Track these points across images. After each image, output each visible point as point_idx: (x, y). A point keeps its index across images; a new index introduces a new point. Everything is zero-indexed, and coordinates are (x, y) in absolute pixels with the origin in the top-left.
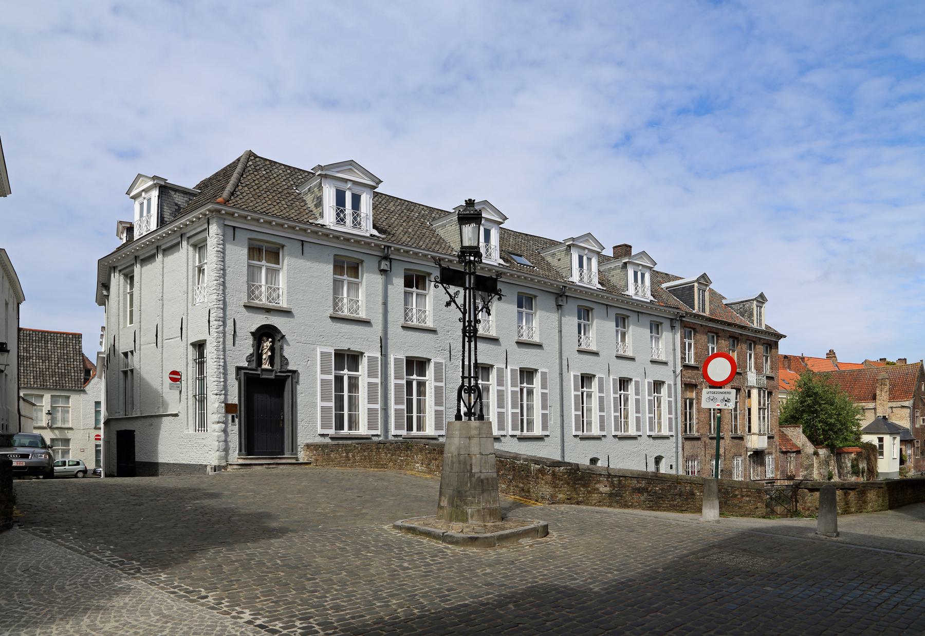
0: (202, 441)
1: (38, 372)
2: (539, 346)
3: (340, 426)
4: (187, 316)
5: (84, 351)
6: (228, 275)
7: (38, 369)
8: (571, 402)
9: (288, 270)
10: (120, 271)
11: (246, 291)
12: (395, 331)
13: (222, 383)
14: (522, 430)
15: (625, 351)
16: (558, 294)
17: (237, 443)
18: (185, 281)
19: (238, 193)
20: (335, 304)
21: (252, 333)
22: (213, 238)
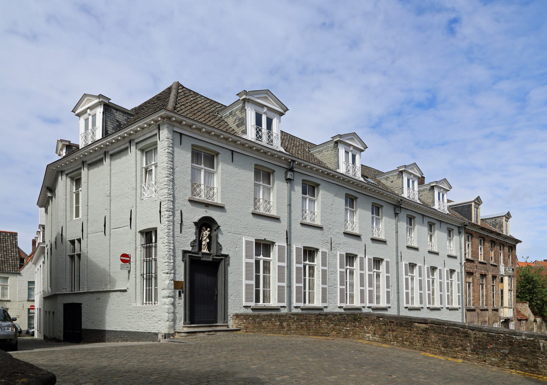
0: (152, 312)
3: (257, 300)
4: (136, 208)
5: (20, 245)
6: (176, 174)
8: (403, 283)
9: (222, 173)
10: (67, 175)
12: (296, 227)
13: (172, 264)
14: (305, 302)
16: (396, 205)
17: (183, 314)
18: (134, 179)
19: (179, 109)
21: (195, 223)
22: (164, 142)
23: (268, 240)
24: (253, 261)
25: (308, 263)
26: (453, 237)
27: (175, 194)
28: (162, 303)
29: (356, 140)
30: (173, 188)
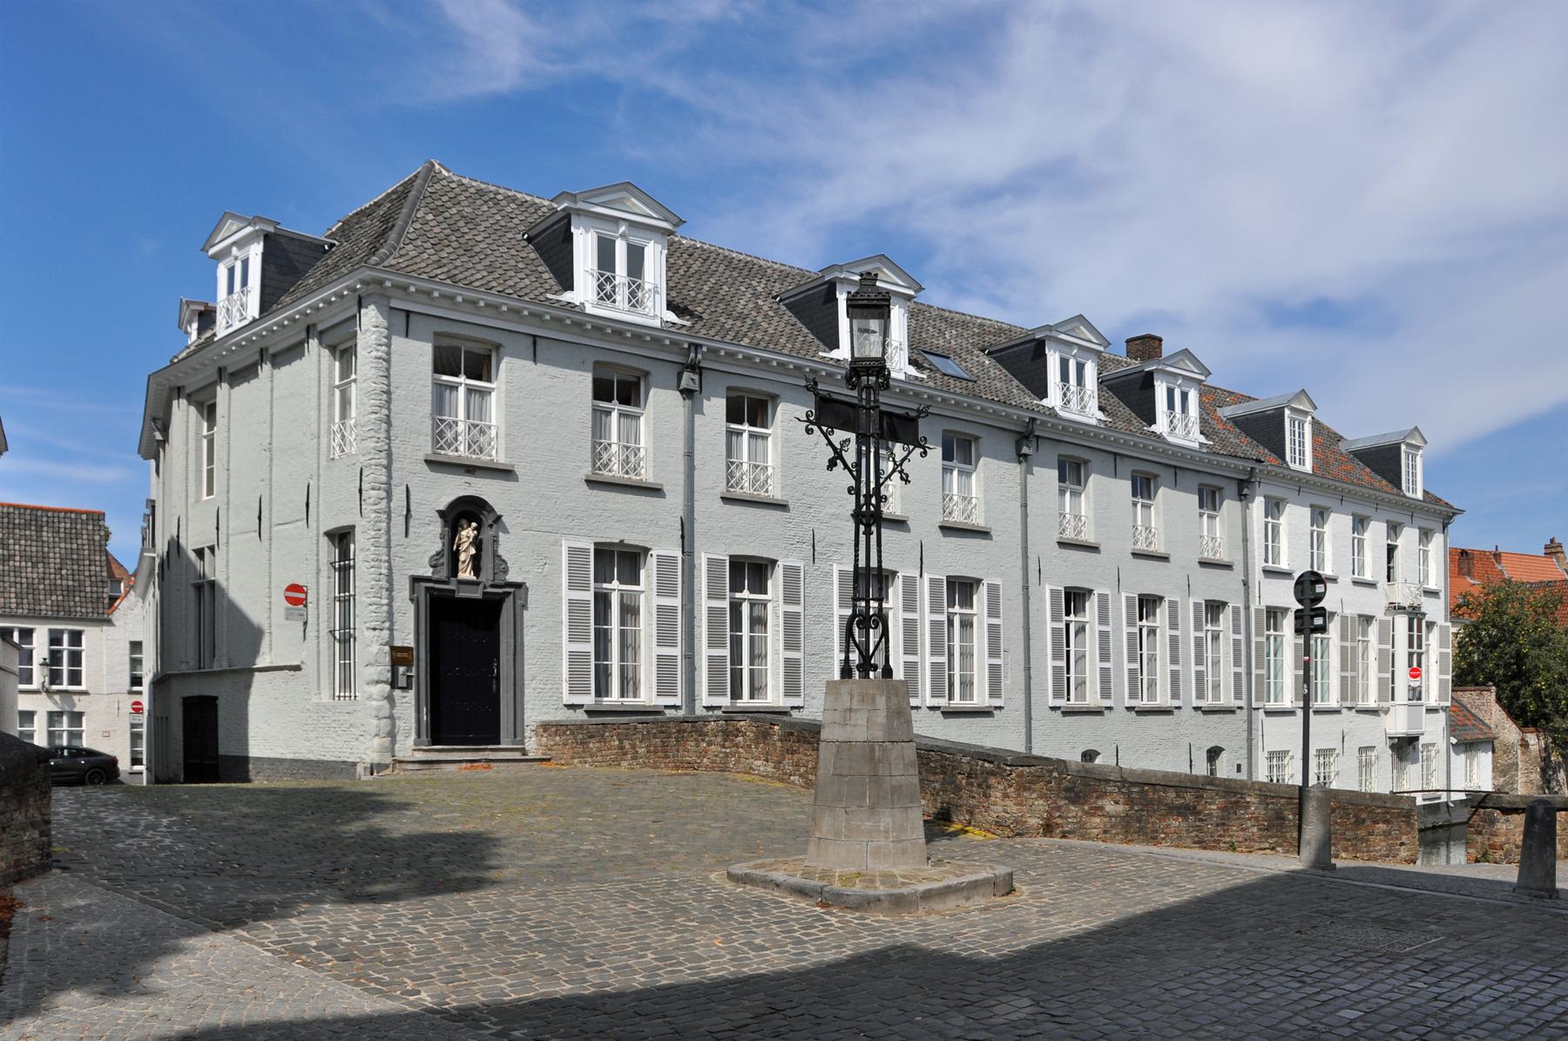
1: (25, 586)
2: (984, 534)
4: (318, 480)
7: (24, 580)
11: (430, 433)
12: (708, 506)
13: (385, 608)
14: (951, 697)
15: (1080, 532)
16: (1020, 433)
17: (413, 721)
18: (314, 414)
20: (596, 456)
21: (441, 514)
23: (631, 543)
24: (589, 596)
25: (746, 597)
26: (1221, 504)
27: (393, 449)
28: (366, 695)
29: (885, 270)
30: (388, 438)
